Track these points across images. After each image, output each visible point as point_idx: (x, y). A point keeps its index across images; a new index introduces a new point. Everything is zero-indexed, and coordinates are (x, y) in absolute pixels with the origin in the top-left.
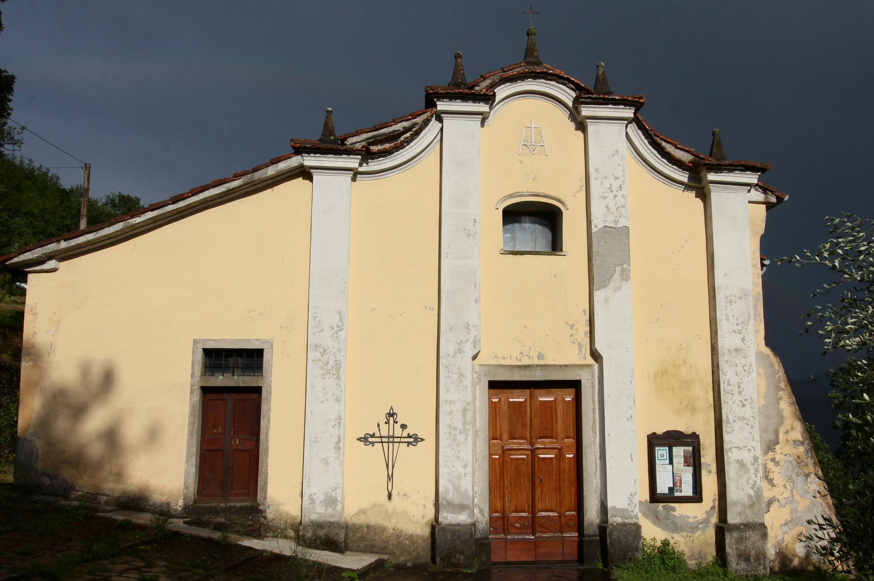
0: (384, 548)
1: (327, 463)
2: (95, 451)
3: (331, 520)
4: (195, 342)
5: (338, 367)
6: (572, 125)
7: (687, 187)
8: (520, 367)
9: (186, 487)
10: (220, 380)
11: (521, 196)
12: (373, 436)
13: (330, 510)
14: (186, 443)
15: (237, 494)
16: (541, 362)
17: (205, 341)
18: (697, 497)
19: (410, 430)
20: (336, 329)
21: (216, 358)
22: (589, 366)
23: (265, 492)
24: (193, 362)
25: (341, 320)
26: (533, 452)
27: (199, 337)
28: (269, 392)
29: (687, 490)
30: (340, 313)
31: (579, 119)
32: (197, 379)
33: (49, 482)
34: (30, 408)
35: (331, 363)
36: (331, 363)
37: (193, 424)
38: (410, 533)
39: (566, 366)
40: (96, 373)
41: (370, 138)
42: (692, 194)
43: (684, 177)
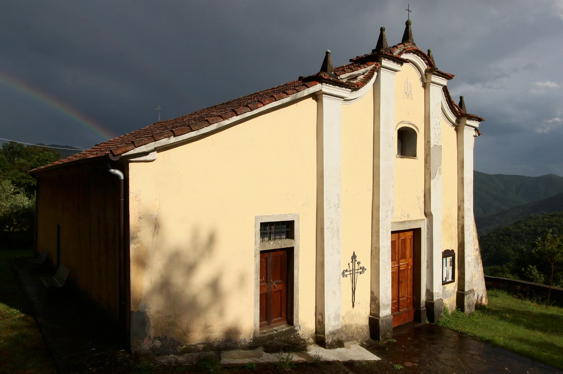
0: (353, 337)
1: (335, 294)
2: (204, 297)
3: (338, 328)
4: (257, 218)
5: (338, 231)
6: (421, 84)
7: (454, 125)
8: (399, 222)
9: (255, 325)
10: (272, 245)
11: (409, 124)
12: (346, 271)
13: (337, 322)
14: (253, 293)
15: (276, 322)
16: (408, 219)
17: (262, 217)
18: (453, 280)
19: (361, 265)
20: (337, 206)
21: (269, 229)
22: (423, 220)
23: (298, 318)
24: (255, 233)
25: (339, 200)
26: (399, 267)
27: (258, 214)
28: (298, 250)
29: (450, 279)
30: (338, 196)
31: (425, 81)
32: (258, 246)
33: (160, 344)
34: (142, 282)
35: (335, 229)
36: (335, 229)
37: (257, 279)
38: (361, 325)
39: (417, 220)
40: (204, 235)
41: (348, 77)
42: (453, 128)
43: (454, 119)
